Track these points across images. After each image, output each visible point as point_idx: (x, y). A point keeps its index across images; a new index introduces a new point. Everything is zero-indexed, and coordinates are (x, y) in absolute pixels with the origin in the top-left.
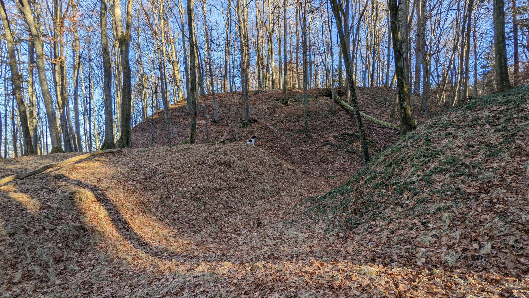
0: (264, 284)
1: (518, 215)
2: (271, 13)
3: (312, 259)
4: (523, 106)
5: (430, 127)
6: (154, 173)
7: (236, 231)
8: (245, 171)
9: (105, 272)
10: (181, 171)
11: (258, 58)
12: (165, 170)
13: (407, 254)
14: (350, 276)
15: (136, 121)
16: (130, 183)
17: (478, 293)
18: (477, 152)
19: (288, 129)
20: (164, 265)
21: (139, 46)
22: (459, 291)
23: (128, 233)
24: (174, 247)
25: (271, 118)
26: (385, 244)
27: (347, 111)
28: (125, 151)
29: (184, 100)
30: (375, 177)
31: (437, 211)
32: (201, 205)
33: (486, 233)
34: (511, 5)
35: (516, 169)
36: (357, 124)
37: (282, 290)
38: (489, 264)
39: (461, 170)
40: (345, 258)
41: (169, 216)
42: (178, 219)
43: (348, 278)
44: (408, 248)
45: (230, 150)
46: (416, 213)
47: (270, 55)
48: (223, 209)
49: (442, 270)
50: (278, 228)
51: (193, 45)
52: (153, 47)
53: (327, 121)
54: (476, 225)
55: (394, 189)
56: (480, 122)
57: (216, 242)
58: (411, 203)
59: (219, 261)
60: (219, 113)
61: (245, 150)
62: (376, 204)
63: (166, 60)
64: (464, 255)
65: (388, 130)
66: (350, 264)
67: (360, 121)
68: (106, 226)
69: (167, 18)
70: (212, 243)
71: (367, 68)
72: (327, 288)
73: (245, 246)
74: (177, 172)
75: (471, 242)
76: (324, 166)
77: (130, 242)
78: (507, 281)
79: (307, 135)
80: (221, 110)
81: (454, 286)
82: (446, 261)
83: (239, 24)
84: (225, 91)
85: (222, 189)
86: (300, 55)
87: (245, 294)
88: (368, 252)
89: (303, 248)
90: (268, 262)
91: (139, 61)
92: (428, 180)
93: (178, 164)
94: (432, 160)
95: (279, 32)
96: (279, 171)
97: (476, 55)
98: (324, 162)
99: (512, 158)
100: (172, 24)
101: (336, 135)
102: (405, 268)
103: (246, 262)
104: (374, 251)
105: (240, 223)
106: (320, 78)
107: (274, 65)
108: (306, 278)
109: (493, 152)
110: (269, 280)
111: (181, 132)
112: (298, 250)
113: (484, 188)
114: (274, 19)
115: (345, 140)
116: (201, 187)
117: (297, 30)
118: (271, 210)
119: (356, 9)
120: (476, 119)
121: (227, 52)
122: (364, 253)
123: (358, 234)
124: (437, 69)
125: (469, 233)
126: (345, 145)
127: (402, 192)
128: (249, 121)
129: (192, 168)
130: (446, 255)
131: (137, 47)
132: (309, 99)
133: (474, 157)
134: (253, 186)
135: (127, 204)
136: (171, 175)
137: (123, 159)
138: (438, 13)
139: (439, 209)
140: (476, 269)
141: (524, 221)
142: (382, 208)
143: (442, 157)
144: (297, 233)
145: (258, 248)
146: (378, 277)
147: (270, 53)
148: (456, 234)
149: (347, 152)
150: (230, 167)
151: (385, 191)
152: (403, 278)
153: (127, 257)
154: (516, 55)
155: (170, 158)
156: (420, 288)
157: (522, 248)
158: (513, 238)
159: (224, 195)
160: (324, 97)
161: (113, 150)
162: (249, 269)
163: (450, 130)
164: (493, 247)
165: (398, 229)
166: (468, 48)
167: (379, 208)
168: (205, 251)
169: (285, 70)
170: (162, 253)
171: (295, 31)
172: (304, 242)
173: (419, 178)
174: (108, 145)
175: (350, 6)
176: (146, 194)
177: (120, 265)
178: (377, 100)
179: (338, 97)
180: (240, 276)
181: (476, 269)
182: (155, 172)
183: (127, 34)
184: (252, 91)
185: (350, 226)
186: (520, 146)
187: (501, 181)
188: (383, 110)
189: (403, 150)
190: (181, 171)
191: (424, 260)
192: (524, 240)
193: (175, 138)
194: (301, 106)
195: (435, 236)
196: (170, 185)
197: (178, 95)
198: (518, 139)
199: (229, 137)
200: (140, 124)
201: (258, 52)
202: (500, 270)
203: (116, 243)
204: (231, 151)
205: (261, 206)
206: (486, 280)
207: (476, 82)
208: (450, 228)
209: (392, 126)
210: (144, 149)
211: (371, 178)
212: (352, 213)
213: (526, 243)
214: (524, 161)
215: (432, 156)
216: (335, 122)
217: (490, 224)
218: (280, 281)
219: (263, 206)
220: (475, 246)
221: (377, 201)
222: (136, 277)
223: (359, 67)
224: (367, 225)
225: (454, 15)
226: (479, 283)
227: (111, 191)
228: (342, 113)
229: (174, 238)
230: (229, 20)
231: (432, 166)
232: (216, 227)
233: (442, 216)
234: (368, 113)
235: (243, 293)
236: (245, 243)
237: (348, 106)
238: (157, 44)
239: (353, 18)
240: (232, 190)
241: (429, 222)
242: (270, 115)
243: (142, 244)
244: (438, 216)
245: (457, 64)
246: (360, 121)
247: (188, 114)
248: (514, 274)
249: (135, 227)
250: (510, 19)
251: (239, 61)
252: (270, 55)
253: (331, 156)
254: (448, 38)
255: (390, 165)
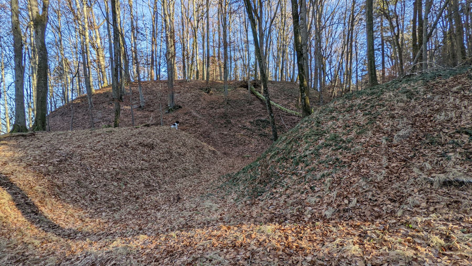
0: (175, 250)
1: (375, 176)
2: (195, 10)
3: (221, 224)
4: (382, 96)
5: (321, 112)
6: (71, 155)
7: (157, 207)
8: (168, 152)
9: (6, 259)
10: (101, 153)
11: (184, 50)
12: (83, 152)
13: (298, 213)
14: (251, 235)
15: (55, 105)
16: (42, 165)
17: (345, 236)
18: (351, 130)
19: (210, 115)
20: (76, 246)
21: (59, 29)
22: (332, 236)
23: (37, 217)
24: (89, 226)
25: (195, 105)
26: (282, 206)
27: (261, 100)
28: (39, 134)
29: (109, 86)
30: (278, 153)
31: (322, 177)
32: (121, 184)
33: (353, 191)
34: (379, 24)
35: (376, 143)
36: (268, 111)
37: (191, 254)
38: (354, 214)
39: (340, 144)
40: (249, 220)
41: (86, 197)
42: (96, 200)
43: (249, 236)
44: (299, 208)
45: (154, 133)
46: (307, 180)
47: (195, 48)
48: (145, 187)
49: (322, 222)
50: (195, 201)
51: (117, 33)
52: (75, 31)
53: (245, 109)
54: (347, 186)
55: (292, 162)
56: (354, 108)
57: (135, 218)
58: (304, 173)
59: (135, 235)
60: (144, 99)
61: (169, 133)
62: (278, 175)
63: (89, 45)
64: (338, 209)
65: (294, 118)
66: (252, 225)
67: (270, 108)
68: (9, 210)
69: (91, 4)
70: (131, 220)
71: (278, 66)
72: (230, 247)
73: (163, 219)
74: (97, 154)
75: (343, 199)
76: (241, 147)
77: (39, 225)
78: (365, 225)
79: (227, 121)
80: (147, 97)
81: (329, 233)
82: (325, 215)
83: (165, 17)
84: (151, 79)
85: (144, 169)
86: (222, 50)
87: (155, 261)
88: (268, 214)
89: (215, 216)
90: (182, 231)
91: (58, 44)
92: (317, 153)
93: (99, 147)
94: (320, 138)
95: (203, 28)
96: (200, 152)
97: (357, 61)
98: (241, 144)
99: (374, 134)
100: (96, 10)
101: (252, 120)
102: (295, 224)
103: (161, 234)
104: (273, 213)
105: (161, 200)
106: (239, 72)
107: (199, 58)
108: (214, 240)
109: (362, 131)
110: (179, 246)
111: (105, 117)
112: (214, 221)
113: (355, 157)
114: (198, 17)
115: (259, 125)
116: (122, 168)
117: (219, 28)
118: (191, 186)
119: (268, 15)
120: (352, 106)
121: (153, 43)
122: (265, 216)
123: (262, 201)
124: (330, 70)
125: (342, 192)
126: (259, 130)
127: (297, 164)
128: (174, 107)
129: (114, 150)
130: (325, 210)
131: (58, 31)
132: (229, 90)
133: (349, 135)
134: (175, 166)
135: (37, 187)
136: (91, 157)
137: (36, 143)
138: (331, 25)
139: (323, 176)
140: (345, 219)
141: (379, 180)
142: (281, 178)
143: (328, 135)
144: (211, 204)
145: (174, 220)
146: (273, 233)
147: (195, 47)
148: (334, 194)
149: (261, 135)
150: (153, 148)
151: (285, 164)
152: (293, 232)
153: (34, 241)
154: (383, 63)
155: (90, 140)
156: (304, 238)
157: (376, 200)
158: (371, 193)
159: (145, 175)
160: (242, 88)
161: (24, 133)
162: (162, 239)
163: (334, 114)
164: (358, 202)
165: (293, 194)
166: (351, 54)
167: (280, 178)
168: (122, 228)
169: (208, 62)
170: (76, 234)
171: (217, 29)
172: (216, 211)
173: (310, 152)
174: (19, 129)
175: (263, 12)
176: (60, 177)
177: (25, 250)
178: (285, 92)
179: (254, 89)
180: (153, 246)
181: (345, 219)
182: (72, 154)
183: (43, 15)
184: (178, 80)
185: (256, 194)
186: (379, 126)
187: (366, 152)
188: (290, 100)
189: (300, 131)
190: (101, 153)
191: (309, 216)
192: (378, 194)
193: (99, 122)
194: (222, 95)
195: (319, 196)
196: (88, 167)
197: (101, 81)
198: (378, 121)
199: (154, 122)
200: (59, 108)
201: (184, 44)
202: (361, 218)
203: (22, 228)
204: (155, 134)
205: (182, 183)
206: (351, 226)
207: (357, 81)
208: (330, 189)
209: (296, 114)
210: (61, 132)
211: (275, 154)
212: (258, 184)
213: (379, 196)
214: (381, 136)
215: (320, 134)
216: (251, 110)
217: (357, 184)
218: (190, 246)
219: (184, 183)
220: (346, 201)
221: (278, 172)
222: (43, 260)
223: (271, 65)
224: (270, 192)
225: (342, 28)
226: (346, 229)
227: (18, 174)
228: (257, 102)
229: (91, 218)
230: (156, 13)
231: (321, 142)
232: (137, 204)
233: (325, 180)
234: (277, 103)
235: (154, 261)
236: (163, 217)
237: (262, 96)
238: (79, 29)
239: (266, 23)
240: (155, 170)
241: (316, 186)
242: (194, 102)
243: (53, 227)
244: (323, 181)
245: (344, 67)
246: (270, 108)
247: (113, 100)
248: (370, 219)
249: (45, 211)
250: (379, 35)
251: (165, 51)
252: (195, 48)
253: (248, 139)
254: (338, 46)
255: (290, 143)
